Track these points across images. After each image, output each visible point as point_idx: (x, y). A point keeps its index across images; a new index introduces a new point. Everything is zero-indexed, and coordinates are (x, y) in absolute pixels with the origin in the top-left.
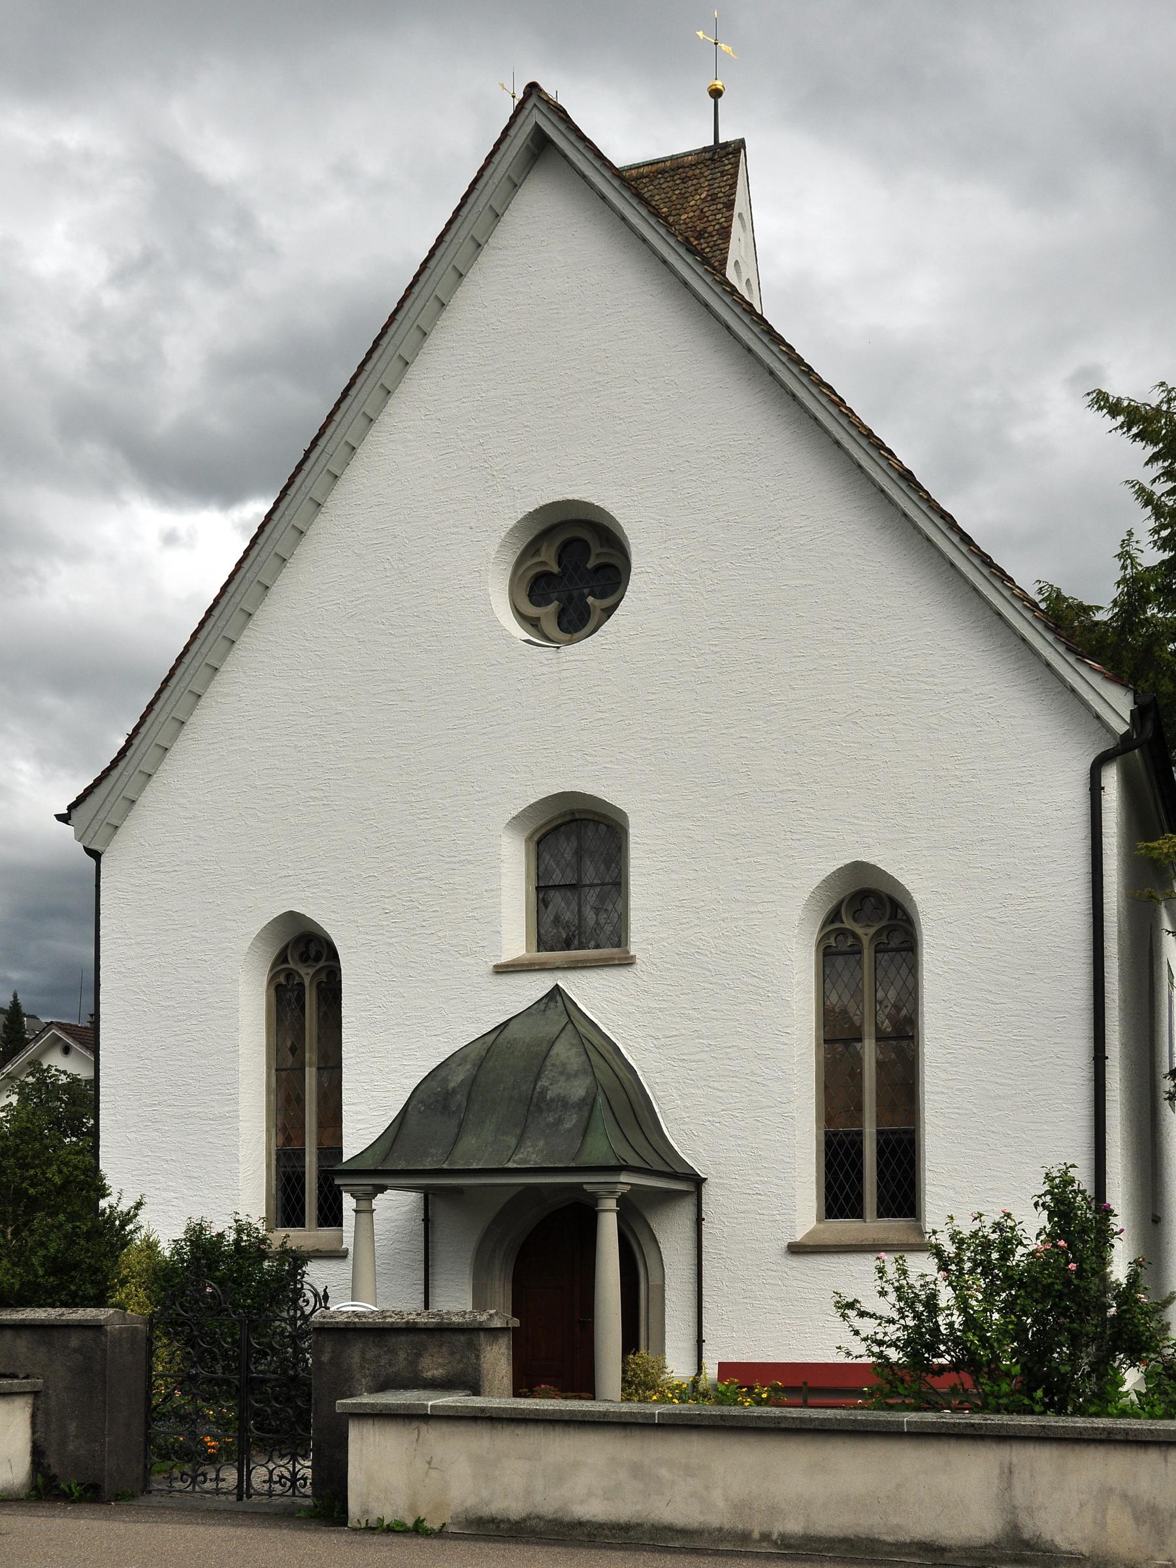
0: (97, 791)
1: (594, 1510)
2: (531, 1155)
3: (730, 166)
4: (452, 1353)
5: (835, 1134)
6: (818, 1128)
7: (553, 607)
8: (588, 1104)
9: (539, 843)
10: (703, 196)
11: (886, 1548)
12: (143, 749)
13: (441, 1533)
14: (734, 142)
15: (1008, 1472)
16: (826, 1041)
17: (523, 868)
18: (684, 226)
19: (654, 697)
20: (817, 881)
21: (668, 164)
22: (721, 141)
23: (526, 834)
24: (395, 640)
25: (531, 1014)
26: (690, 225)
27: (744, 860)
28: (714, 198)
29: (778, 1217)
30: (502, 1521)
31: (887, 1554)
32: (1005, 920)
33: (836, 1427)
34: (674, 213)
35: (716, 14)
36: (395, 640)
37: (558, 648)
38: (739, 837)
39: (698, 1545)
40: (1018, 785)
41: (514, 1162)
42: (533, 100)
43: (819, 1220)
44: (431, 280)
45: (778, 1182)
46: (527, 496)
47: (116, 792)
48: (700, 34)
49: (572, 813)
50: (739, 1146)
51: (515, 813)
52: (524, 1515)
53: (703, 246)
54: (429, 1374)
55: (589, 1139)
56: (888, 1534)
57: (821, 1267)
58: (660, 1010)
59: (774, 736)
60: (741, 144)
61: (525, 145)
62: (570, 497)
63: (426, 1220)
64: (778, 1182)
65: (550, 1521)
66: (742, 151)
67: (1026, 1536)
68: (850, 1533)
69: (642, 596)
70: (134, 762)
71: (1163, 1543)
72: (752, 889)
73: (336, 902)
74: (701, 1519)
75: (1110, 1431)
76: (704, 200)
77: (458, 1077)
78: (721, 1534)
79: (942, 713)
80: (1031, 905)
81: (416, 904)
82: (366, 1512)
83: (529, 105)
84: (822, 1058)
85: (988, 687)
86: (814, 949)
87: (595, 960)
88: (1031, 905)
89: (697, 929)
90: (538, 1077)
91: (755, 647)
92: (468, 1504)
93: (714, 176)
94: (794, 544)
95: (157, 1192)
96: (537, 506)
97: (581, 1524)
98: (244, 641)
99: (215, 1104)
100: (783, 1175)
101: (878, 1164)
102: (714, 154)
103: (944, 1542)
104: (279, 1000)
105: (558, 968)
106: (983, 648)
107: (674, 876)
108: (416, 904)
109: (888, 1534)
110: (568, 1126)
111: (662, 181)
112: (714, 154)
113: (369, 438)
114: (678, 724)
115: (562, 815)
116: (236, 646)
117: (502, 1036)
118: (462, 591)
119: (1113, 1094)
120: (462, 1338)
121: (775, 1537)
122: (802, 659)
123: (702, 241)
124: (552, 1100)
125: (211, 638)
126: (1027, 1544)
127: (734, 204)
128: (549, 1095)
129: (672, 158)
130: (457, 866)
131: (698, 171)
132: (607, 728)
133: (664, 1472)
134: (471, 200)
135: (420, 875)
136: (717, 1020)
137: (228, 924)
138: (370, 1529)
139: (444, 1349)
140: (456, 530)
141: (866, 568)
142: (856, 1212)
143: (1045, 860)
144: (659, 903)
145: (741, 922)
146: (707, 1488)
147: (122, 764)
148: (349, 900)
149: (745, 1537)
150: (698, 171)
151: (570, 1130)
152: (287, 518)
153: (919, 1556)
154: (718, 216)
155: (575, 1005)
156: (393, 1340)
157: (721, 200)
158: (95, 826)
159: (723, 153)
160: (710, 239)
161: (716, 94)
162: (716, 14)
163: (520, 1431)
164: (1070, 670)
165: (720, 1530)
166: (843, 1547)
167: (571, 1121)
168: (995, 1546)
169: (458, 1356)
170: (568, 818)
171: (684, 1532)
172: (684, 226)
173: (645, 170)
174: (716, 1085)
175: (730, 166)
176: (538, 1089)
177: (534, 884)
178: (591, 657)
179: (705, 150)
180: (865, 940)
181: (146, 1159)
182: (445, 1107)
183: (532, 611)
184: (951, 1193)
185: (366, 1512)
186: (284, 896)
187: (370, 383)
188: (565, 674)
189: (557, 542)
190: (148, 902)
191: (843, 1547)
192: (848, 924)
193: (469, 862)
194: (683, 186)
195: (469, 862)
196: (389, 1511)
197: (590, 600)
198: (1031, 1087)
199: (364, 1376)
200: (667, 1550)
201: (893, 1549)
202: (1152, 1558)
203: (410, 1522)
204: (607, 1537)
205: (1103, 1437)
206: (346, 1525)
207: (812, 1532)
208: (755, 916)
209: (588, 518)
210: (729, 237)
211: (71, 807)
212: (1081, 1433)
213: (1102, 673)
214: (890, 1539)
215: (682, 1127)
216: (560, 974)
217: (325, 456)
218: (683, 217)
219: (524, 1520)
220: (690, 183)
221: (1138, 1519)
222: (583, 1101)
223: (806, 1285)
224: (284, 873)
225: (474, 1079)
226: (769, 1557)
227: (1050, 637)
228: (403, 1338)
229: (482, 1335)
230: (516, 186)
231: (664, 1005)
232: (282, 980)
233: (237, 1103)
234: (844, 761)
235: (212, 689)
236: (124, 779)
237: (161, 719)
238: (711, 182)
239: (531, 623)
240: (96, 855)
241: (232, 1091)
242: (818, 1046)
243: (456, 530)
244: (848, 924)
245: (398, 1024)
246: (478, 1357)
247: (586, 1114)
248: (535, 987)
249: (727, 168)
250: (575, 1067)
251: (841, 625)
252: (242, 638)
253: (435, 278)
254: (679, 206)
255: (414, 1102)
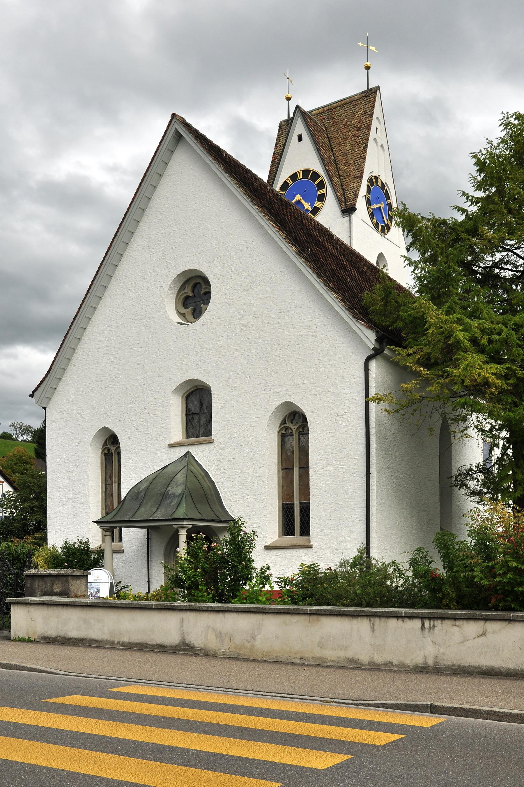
0: (41, 386)
1: (74, 634)
2: (159, 515)
3: (372, 98)
4: (62, 584)
5: (286, 504)
6: (279, 502)
7: (190, 309)
8: (182, 495)
9: (187, 398)
10: (361, 112)
11: (150, 646)
12: (55, 370)
13: (34, 642)
14: (375, 88)
15: (182, 621)
16: (282, 469)
17: (180, 408)
18: (353, 126)
19: (219, 342)
20: (273, 409)
21: (348, 100)
22: (370, 88)
23: (181, 395)
24: (136, 325)
25: (176, 462)
26: (355, 125)
27: (249, 402)
28: (365, 112)
29: (262, 536)
30: (50, 638)
31: (150, 648)
32: (337, 421)
33: (135, 606)
34: (349, 121)
35: (367, 34)
36: (136, 325)
37: (188, 325)
38: (247, 394)
39: (101, 645)
40: (341, 369)
41: (153, 518)
42: (174, 120)
43: (279, 537)
44: (143, 190)
45: (262, 523)
46: (178, 269)
47: (48, 386)
48: (360, 44)
49: (196, 386)
50: (248, 509)
51: (174, 388)
52: (56, 636)
53: (360, 134)
54: (56, 591)
55: (178, 509)
56: (150, 641)
57: (276, 554)
58: (222, 459)
59: (259, 355)
60: (378, 88)
61: (173, 137)
62: (191, 268)
63: (148, 538)
64: (262, 523)
65: (63, 638)
66: (378, 91)
67: (187, 642)
68: (140, 641)
69: (215, 304)
70: (53, 375)
71: (223, 644)
72: (252, 413)
73: (118, 423)
74: (102, 637)
75: (207, 607)
76: (361, 114)
77: (144, 486)
78: (107, 642)
79: (315, 343)
80: (345, 416)
81: (143, 423)
82: (15, 635)
83: (173, 122)
84: (280, 476)
85: (330, 332)
86: (277, 434)
87: (201, 441)
88: (345, 416)
89: (234, 429)
90: (168, 486)
91: (252, 321)
92: (41, 632)
93: (366, 103)
94: (265, 281)
95: (65, 530)
96: (181, 272)
97: (71, 639)
98: (89, 328)
99: (82, 497)
100: (263, 520)
101: (300, 516)
102: (366, 94)
103: (165, 644)
104: (106, 459)
105: (188, 445)
106: (328, 317)
107: (226, 409)
108: (143, 423)
109: (150, 641)
110: (173, 504)
111: (346, 107)
112: (366, 94)
113: (127, 250)
114: (227, 352)
115: (193, 387)
116: (86, 330)
117: (162, 472)
118: (157, 305)
119: (374, 487)
120: (64, 578)
121: (121, 643)
122: (268, 325)
123: (360, 131)
124: (171, 494)
125: (76, 328)
126: (187, 645)
127: (373, 115)
128: (170, 492)
129: (350, 97)
130: (156, 408)
131: (360, 102)
132: (204, 354)
133: (92, 622)
134: (155, 159)
135: (145, 412)
136: (241, 462)
137: (85, 432)
138: (15, 640)
139: (60, 582)
140: (155, 283)
141: (289, 289)
142: (292, 534)
143: (350, 398)
144: (222, 419)
145: (248, 426)
146: (103, 627)
147: (49, 376)
148: (123, 422)
149: (113, 643)
150: (360, 102)
151: (174, 505)
152: (98, 282)
153: (159, 649)
154: (366, 120)
155: (194, 458)
156: (46, 579)
157: (368, 113)
158: (41, 398)
159: (370, 93)
160: (363, 130)
161: (368, 68)
162: (367, 34)
163: (55, 608)
164: (354, 325)
165: (107, 640)
166: (139, 646)
167: (175, 502)
168: (178, 645)
169: (63, 585)
170: (195, 388)
171: (97, 641)
172: (353, 126)
173: (339, 104)
174: (241, 487)
175: (372, 98)
176: (167, 491)
177: (185, 413)
178: (199, 328)
179: (363, 92)
180: (294, 431)
181: (61, 518)
182: (137, 498)
183: (183, 311)
184: (319, 526)
185: (15, 635)
186: (102, 421)
187: (124, 230)
188: (191, 335)
189: (191, 285)
190: (61, 425)
191: (139, 646)
192: (289, 424)
193: (160, 406)
194: (353, 108)
195: (160, 406)
196: (22, 634)
197: (202, 305)
198: (345, 485)
199: (39, 591)
200: (93, 647)
201: (152, 646)
202: (220, 649)
203: (27, 638)
204: (77, 643)
205: (206, 609)
206: (10, 639)
207: (131, 641)
208: (252, 423)
209: (200, 275)
210: (370, 129)
211: (34, 392)
212: (200, 608)
213: (365, 326)
214: (151, 643)
215: (230, 503)
216: (190, 447)
217: (110, 259)
218: (353, 122)
219: (56, 637)
220: (356, 107)
221: (216, 636)
222: (180, 494)
223: (271, 561)
224: (102, 413)
225: (148, 488)
226: (119, 649)
227: (347, 312)
228: (49, 579)
229: (70, 578)
230: (172, 152)
231: (223, 457)
232: (106, 451)
233: (89, 497)
234: (282, 363)
235: (80, 346)
236: (50, 381)
237: (61, 359)
238: (364, 106)
239: (182, 315)
240: (45, 408)
241: (87, 493)
242: (278, 471)
243: (155, 283)
244: (289, 424)
245: (138, 467)
246: (69, 585)
247: (180, 499)
248: (181, 452)
249: (371, 99)
250: (181, 482)
251: (281, 311)
252: (88, 327)
253: (144, 189)
254: (351, 118)
255: (128, 496)
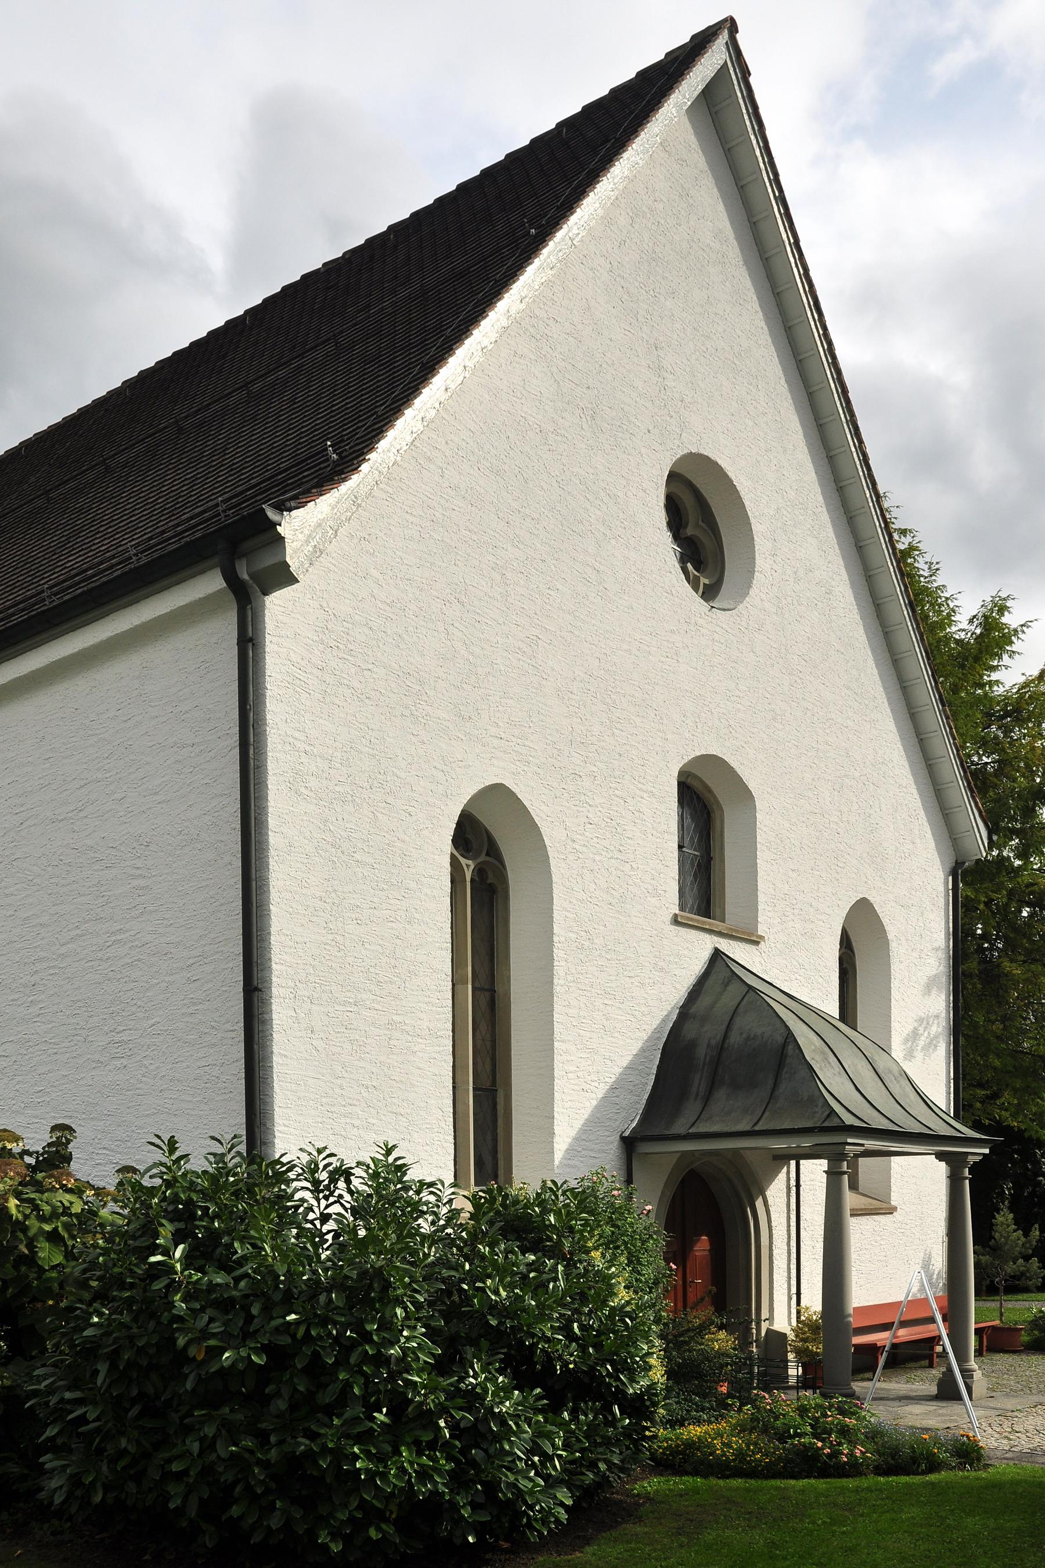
181: (339, 1082)
